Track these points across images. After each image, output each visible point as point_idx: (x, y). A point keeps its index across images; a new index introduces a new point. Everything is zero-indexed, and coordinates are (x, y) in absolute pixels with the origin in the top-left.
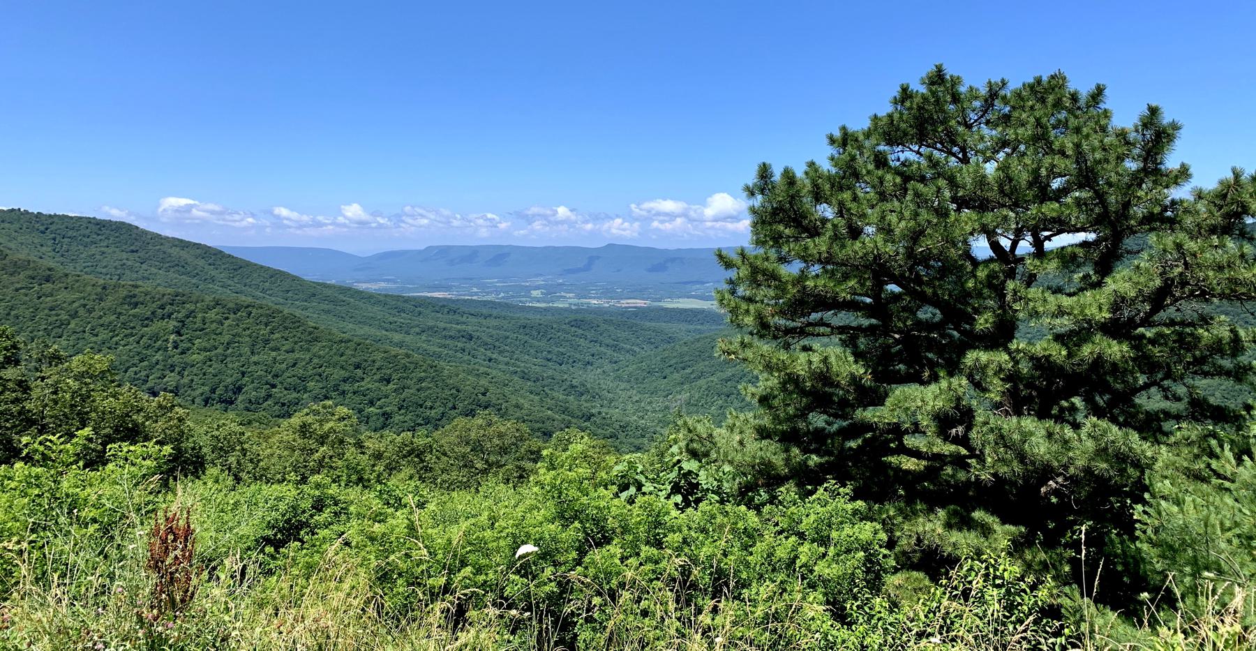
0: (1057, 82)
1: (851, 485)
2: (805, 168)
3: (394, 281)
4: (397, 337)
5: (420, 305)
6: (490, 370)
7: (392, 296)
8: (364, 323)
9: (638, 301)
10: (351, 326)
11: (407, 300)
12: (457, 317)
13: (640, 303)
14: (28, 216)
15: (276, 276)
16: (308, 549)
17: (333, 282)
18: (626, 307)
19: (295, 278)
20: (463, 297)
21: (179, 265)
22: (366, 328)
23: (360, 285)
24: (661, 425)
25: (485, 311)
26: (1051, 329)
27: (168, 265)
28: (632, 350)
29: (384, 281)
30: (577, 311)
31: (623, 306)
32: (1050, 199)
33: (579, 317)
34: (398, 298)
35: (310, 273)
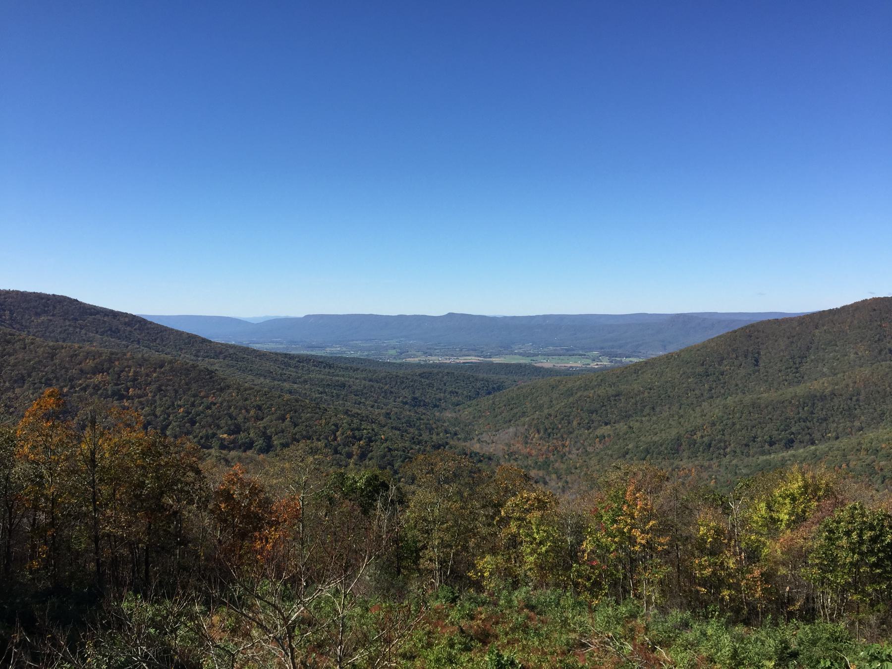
6: (515, 411)
7: (280, 354)
8: (261, 375)
9: (473, 358)
10: (250, 377)
11: (292, 357)
12: (332, 371)
13: (474, 359)
14: (77, 303)
17: (233, 343)
18: (464, 363)
19: (204, 341)
20: (335, 355)
21: (114, 332)
25: (354, 365)
26: (747, 430)
27: (103, 330)
28: (319, 394)
29: (273, 342)
33: (426, 370)
35: (218, 337)
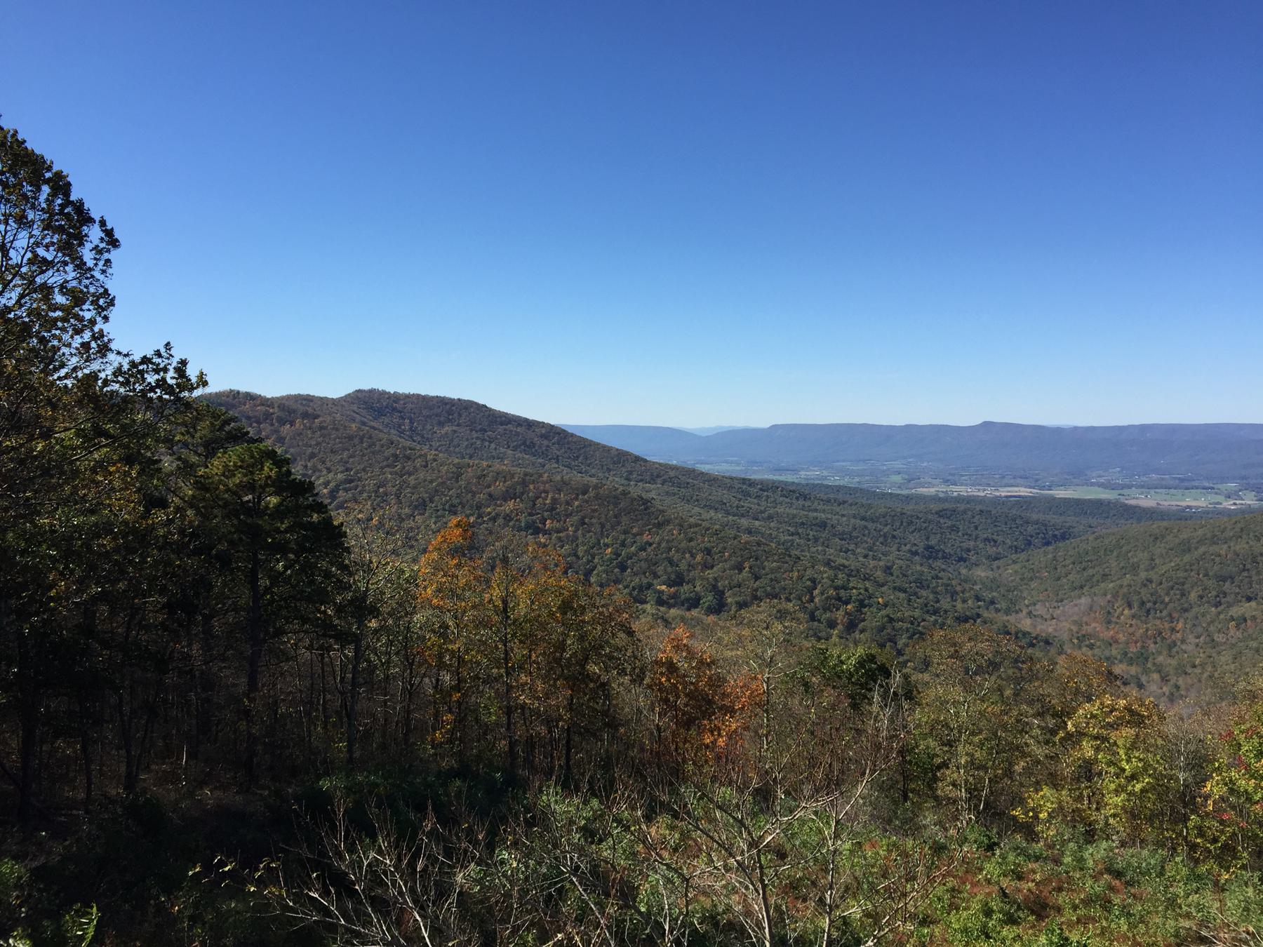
0: (145, 357)
1: (239, 473)
2: (198, 373)
3: (738, 464)
4: (744, 522)
5: (767, 488)
7: (737, 479)
8: (711, 507)
9: (1022, 489)
10: (697, 510)
11: (752, 483)
13: (1023, 491)
15: (620, 459)
16: (242, 552)
18: (1006, 497)
19: (637, 459)
21: (528, 447)
22: (712, 513)
23: (702, 466)
24: (918, 584)
25: (840, 497)
29: (726, 462)
30: (945, 500)
31: (1003, 494)
32: (196, 388)
34: (744, 481)
35: (656, 454)
